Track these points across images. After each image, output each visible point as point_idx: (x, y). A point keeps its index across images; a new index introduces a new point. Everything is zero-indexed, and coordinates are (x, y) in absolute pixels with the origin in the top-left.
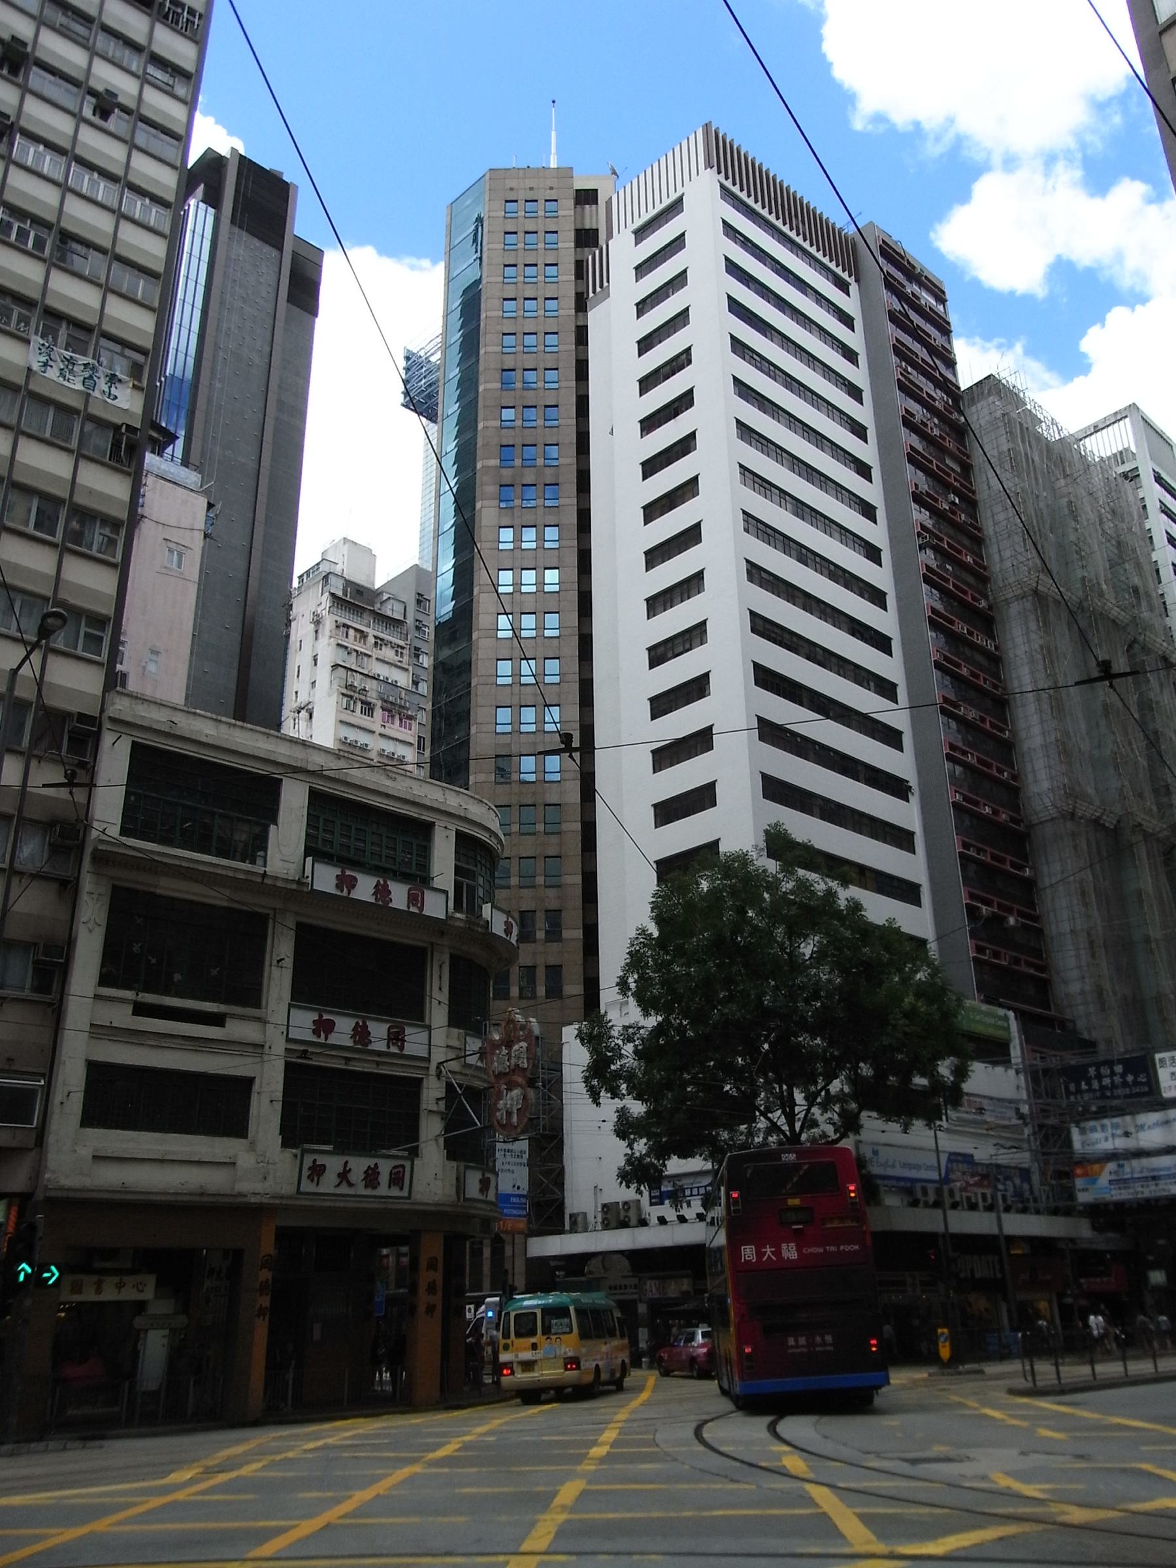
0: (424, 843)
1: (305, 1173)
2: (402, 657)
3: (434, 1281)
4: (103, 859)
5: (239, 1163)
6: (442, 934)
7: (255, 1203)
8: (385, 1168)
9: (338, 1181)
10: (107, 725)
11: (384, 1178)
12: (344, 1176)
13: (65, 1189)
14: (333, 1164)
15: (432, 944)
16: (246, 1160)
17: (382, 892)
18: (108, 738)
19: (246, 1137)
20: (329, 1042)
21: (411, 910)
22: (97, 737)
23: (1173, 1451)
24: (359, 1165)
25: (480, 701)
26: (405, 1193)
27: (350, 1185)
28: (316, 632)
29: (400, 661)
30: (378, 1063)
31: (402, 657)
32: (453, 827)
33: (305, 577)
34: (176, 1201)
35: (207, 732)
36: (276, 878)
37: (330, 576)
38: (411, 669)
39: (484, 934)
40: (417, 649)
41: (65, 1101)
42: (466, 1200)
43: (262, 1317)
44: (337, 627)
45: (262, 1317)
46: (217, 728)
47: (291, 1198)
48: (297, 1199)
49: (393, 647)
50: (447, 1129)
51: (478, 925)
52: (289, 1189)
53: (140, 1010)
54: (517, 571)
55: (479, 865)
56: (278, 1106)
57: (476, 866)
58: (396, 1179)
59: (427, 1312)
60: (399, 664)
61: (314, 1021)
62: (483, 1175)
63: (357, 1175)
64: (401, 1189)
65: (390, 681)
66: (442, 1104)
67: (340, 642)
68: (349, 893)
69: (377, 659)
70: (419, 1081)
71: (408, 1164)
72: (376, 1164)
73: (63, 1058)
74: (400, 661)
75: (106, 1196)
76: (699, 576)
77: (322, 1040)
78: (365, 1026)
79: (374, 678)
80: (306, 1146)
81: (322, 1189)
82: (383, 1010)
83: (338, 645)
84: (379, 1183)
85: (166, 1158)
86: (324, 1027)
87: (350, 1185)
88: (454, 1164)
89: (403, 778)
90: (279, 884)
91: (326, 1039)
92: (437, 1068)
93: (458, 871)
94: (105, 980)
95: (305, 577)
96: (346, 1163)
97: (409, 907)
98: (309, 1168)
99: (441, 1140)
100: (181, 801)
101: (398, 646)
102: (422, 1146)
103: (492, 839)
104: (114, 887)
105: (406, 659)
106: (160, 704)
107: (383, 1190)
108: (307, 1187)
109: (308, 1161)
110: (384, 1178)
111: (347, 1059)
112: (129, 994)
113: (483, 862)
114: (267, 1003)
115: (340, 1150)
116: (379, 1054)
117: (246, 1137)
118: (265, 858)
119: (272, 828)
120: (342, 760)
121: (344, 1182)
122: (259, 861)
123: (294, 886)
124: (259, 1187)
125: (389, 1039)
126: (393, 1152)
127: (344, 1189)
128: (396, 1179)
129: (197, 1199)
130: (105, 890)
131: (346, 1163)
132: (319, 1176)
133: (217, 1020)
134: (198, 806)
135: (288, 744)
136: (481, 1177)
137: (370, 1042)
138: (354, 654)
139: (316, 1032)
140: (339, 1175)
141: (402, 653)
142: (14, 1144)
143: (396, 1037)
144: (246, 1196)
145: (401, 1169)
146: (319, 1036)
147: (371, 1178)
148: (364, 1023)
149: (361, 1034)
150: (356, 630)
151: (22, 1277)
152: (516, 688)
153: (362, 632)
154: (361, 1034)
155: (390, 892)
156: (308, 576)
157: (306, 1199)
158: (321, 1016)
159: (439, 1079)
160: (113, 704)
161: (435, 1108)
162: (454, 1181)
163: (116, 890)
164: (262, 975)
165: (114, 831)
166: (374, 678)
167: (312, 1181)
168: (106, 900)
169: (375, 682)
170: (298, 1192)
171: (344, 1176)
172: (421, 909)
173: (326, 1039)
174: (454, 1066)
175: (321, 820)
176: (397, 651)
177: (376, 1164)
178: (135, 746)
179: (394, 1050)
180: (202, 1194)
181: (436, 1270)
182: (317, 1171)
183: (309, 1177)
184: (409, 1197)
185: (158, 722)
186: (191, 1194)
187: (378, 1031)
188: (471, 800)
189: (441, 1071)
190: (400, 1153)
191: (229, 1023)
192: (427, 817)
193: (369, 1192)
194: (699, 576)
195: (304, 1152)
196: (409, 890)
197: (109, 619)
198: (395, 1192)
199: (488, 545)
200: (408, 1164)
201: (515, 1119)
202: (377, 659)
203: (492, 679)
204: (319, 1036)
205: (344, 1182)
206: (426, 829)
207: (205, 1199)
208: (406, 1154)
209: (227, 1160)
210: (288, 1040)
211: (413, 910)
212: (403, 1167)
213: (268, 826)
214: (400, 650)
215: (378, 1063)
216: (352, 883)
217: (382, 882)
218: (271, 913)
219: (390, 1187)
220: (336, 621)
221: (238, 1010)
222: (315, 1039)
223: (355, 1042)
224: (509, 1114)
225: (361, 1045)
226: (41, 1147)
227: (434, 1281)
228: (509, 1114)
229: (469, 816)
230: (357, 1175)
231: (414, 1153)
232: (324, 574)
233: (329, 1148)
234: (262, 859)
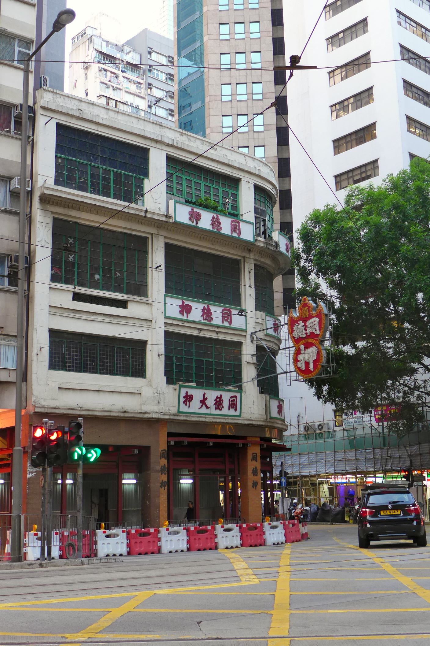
0: (235, 192)
1: (182, 400)
2: (140, 90)
3: (256, 467)
4: (46, 200)
5: (143, 394)
6: (250, 251)
7: (155, 418)
8: (226, 397)
9: (201, 405)
10: (39, 111)
11: (226, 404)
12: (203, 402)
13: (45, 407)
14: (197, 394)
15: (244, 257)
16: (147, 392)
17: (215, 222)
18: (41, 120)
19: (145, 378)
20: (189, 318)
21: (233, 235)
22: (33, 120)
23: (1, 569)
24: (212, 395)
25: (212, 112)
26: (238, 413)
27: (207, 407)
28: (86, 74)
29: (140, 93)
30: (217, 333)
31: (140, 90)
32: (252, 182)
33: (76, 39)
34: (110, 416)
35: (102, 116)
36: (153, 213)
37: (93, 37)
38: (146, 97)
39: (275, 251)
40: (150, 84)
41: (39, 353)
42: (271, 418)
43: (163, 488)
44: (100, 71)
45: (163, 488)
46: (107, 114)
47: (174, 415)
48: (178, 415)
49: (134, 84)
50: (258, 375)
51: (271, 245)
52: (174, 410)
53: (77, 297)
54: (232, 24)
55: (267, 207)
56: (163, 358)
57: (266, 208)
58: (233, 405)
59: (253, 487)
60: (139, 94)
61: (180, 306)
62: (279, 403)
63: (210, 402)
64: (236, 410)
65: (134, 106)
66: (255, 358)
67: (103, 81)
68: (197, 224)
69: (126, 92)
70: (240, 344)
71: (238, 395)
72: (221, 395)
73: (35, 327)
74: (140, 93)
75: (62, 411)
76: (364, 21)
77: (185, 317)
78: (209, 309)
79: (124, 103)
80: (181, 383)
81: (191, 410)
82: (218, 299)
83: (101, 82)
84: (223, 407)
85: (100, 389)
86: (185, 309)
87: (207, 407)
88: (263, 395)
89: (221, 148)
90: (155, 217)
91: (187, 317)
92: (251, 336)
93: (256, 211)
94: (54, 278)
95: (76, 39)
96: (204, 394)
97: (232, 234)
98: (184, 397)
99: (256, 382)
100: (90, 163)
101: (138, 83)
102: (244, 385)
103: (274, 190)
104: (55, 219)
105: (143, 91)
106: (71, 98)
107: (226, 411)
108: (184, 408)
109: (183, 392)
110: (226, 404)
111: (200, 330)
112: (70, 287)
113: (269, 205)
114: (152, 293)
115: (200, 385)
116: (218, 327)
117: (145, 378)
118: (143, 200)
119: (146, 181)
120: (184, 136)
121: (204, 406)
122: (140, 202)
123: (164, 219)
124: (156, 408)
125: (223, 317)
126: (230, 388)
127: (204, 410)
128: (233, 405)
129: (122, 415)
130: (50, 221)
131: (204, 394)
132: (190, 402)
133: (123, 304)
134: (100, 166)
135: (151, 125)
136: (278, 404)
137: (212, 319)
138: (111, 88)
139: (181, 312)
140: (201, 401)
141: (140, 87)
142: (10, 380)
143: (226, 316)
144: (150, 413)
145: (235, 399)
146: (183, 315)
147: (219, 402)
148: (208, 307)
149: (207, 314)
150: (112, 72)
151: (76, 457)
152: (234, 103)
153: (114, 73)
154: (207, 314)
155: (220, 223)
156: (78, 38)
157: (184, 416)
158: (183, 302)
159: (252, 343)
160: (42, 97)
161: (251, 361)
162: (264, 407)
163: (55, 221)
164: (146, 275)
165: (51, 182)
166: (124, 103)
167: (186, 405)
168: (51, 226)
169: (125, 106)
170: (179, 412)
171: (203, 402)
172: (239, 234)
173: (187, 317)
174: (261, 335)
175: (174, 176)
176: (137, 86)
177: (221, 395)
178: (59, 126)
179: (226, 324)
180: (125, 412)
181: (256, 461)
182: (189, 398)
183: (184, 402)
184: (240, 416)
185: (72, 109)
186: (119, 412)
187: (217, 311)
188: (261, 164)
189: (253, 338)
190: (232, 389)
191: (130, 305)
192: (236, 174)
193: (218, 412)
194: (364, 21)
195: (180, 387)
196: (232, 222)
197: (33, 42)
198: (232, 412)
199: (211, 8)
200: (238, 395)
201: (311, 367)
202: (126, 92)
203: (219, 98)
204: (183, 315)
205: (204, 406)
206: (236, 182)
207: (126, 415)
208: (236, 389)
209: (136, 392)
210: (166, 317)
211: (235, 235)
212: (236, 397)
213: (143, 179)
214: (139, 85)
215: (217, 333)
216: (198, 217)
217: (215, 217)
218: (150, 236)
219: (229, 409)
220: (99, 67)
221: (136, 298)
222: (180, 316)
223: (204, 320)
224: (307, 364)
225: (208, 321)
226: (26, 381)
227: (256, 467)
228: (307, 364)
229: (262, 175)
230: (210, 402)
231: (240, 388)
232: (89, 36)
233: (194, 384)
234: (141, 201)
